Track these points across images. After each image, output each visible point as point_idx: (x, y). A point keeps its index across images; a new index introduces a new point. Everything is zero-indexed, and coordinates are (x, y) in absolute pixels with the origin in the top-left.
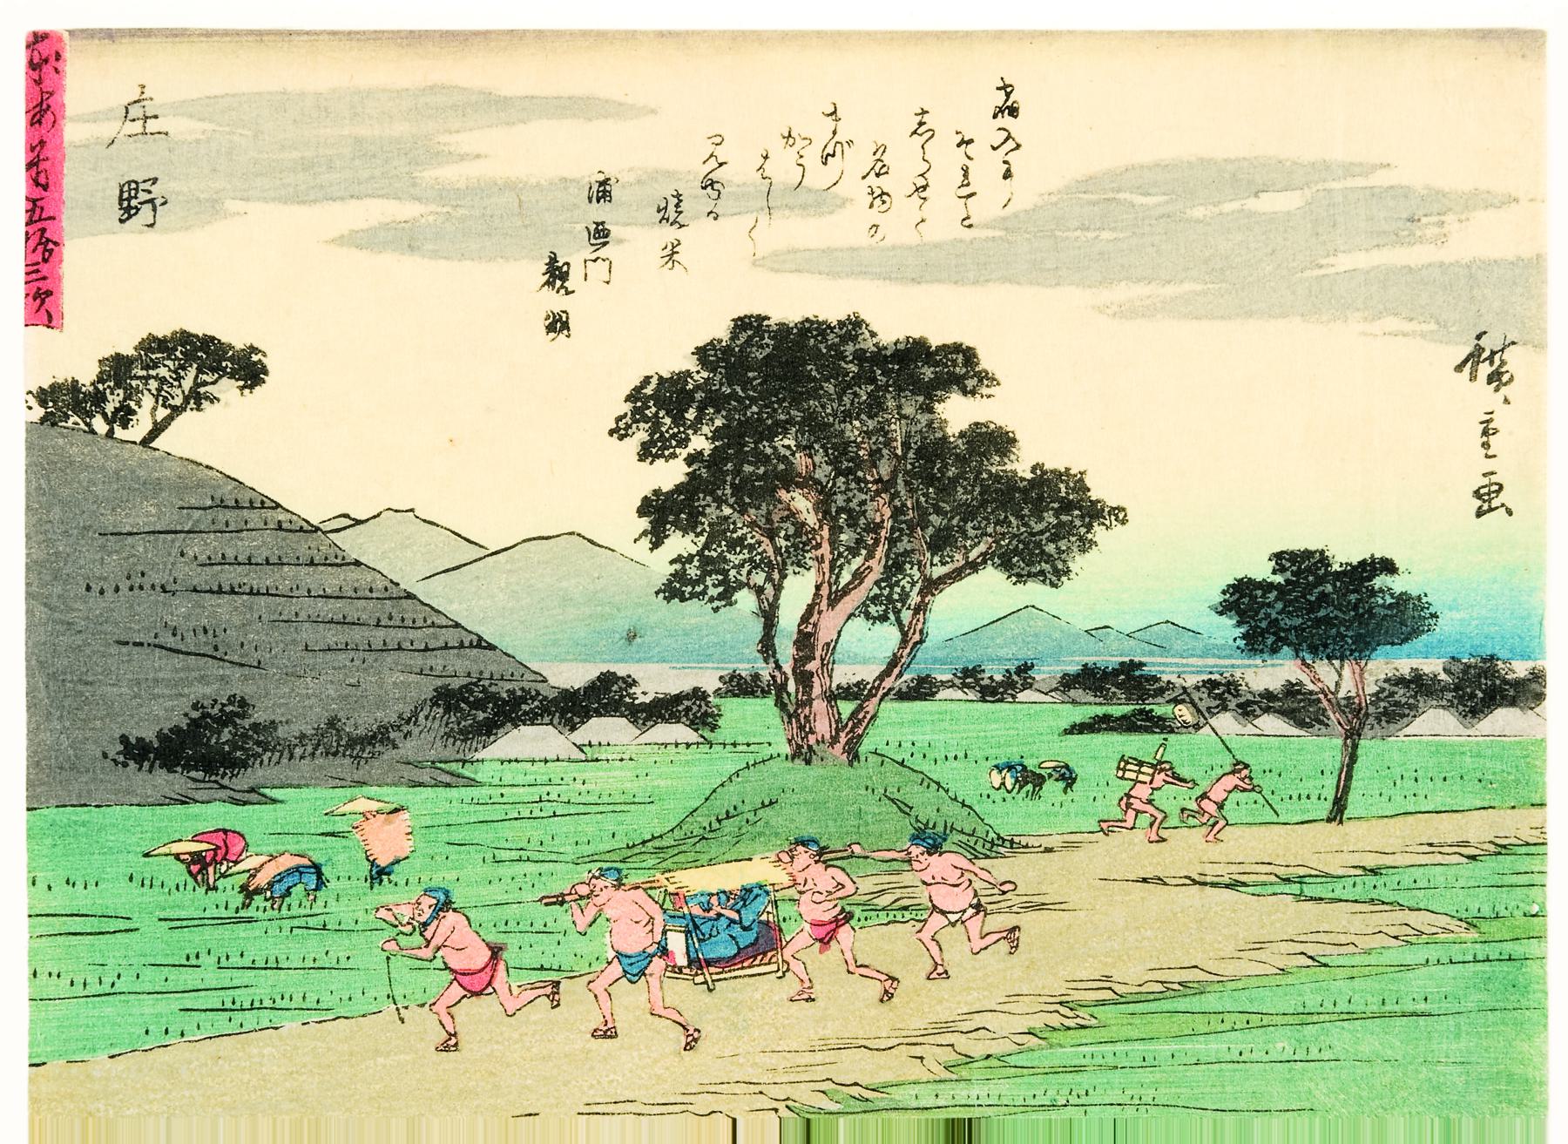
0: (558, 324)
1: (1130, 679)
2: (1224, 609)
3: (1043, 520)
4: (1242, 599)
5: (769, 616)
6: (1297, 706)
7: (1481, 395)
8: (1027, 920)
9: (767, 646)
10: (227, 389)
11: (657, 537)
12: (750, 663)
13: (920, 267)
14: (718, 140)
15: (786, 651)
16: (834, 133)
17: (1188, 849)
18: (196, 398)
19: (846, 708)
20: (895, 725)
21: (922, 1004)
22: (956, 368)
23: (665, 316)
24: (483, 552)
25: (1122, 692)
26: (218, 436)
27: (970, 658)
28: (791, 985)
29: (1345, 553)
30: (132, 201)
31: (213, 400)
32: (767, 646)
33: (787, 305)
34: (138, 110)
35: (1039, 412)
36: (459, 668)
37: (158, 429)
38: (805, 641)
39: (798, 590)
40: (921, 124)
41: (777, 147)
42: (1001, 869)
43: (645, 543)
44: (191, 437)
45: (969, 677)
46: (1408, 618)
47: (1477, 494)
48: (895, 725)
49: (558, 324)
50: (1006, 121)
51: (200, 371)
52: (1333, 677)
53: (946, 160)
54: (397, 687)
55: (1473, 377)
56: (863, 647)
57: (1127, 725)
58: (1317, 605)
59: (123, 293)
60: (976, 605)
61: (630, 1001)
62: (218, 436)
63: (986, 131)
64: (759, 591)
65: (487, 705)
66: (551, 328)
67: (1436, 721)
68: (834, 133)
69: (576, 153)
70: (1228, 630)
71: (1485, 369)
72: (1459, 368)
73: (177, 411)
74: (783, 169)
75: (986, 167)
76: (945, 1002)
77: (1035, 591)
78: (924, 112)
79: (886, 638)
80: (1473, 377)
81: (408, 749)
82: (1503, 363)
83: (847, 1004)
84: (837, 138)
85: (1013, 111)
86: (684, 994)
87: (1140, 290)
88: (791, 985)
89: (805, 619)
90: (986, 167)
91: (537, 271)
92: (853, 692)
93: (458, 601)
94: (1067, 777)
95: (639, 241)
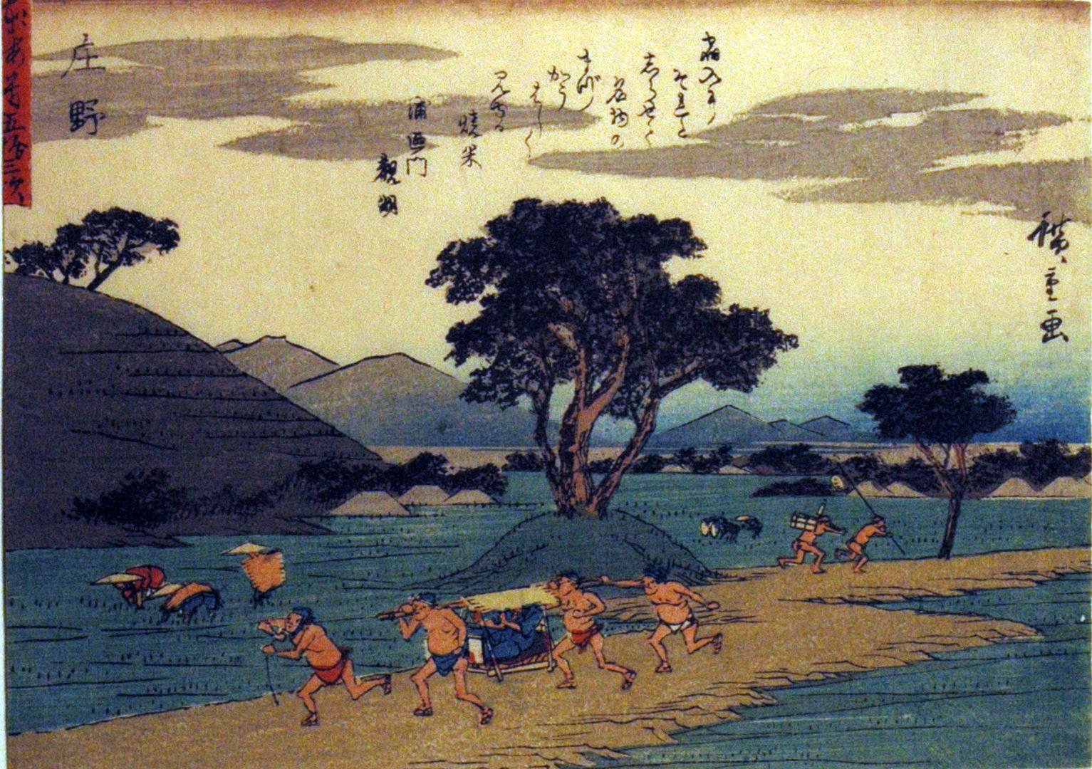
0: (388, 205)
3: (743, 343)
4: (878, 399)
5: (541, 411)
6: (916, 475)
7: (1047, 256)
8: (731, 630)
11: (460, 356)
14: (502, 75)
15: (554, 437)
16: (587, 70)
17: (841, 578)
18: (129, 257)
19: (598, 479)
22: (678, 237)
25: (793, 464)
26: (141, 283)
29: (953, 366)
30: (82, 118)
36: (317, 450)
37: (100, 278)
38: (568, 430)
39: (563, 394)
40: (649, 64)
41: (545, 80)
42: (708, 593)
47: (1043, 326)
48: (634, 491)
49: (388, 205)
50: (710, 63)
51: (130, 237)
52: (945, 456)
54: (272, 461)
55: (1041, 244)
56: (611, 433)
60: (691, 401)
61: (442, 690)
62: (141, 283)
63: (696, 70)
64: (534, 395)
66: (383, 208)
68: (587, 70)
70: (869, 422)
71: (1049, 238)
72: (1031, 237)
73: (113, 266)
75: (696, 94)
76: (672, 688)
78: (651, 56)
79: (628, 427)
80: (1041, 244)
81: (283, 507)
84: (589, 74)
85: (715, 56)
88: (558, 677)
89: (569, 413)
90: (696, 94)
94: (755, 527)
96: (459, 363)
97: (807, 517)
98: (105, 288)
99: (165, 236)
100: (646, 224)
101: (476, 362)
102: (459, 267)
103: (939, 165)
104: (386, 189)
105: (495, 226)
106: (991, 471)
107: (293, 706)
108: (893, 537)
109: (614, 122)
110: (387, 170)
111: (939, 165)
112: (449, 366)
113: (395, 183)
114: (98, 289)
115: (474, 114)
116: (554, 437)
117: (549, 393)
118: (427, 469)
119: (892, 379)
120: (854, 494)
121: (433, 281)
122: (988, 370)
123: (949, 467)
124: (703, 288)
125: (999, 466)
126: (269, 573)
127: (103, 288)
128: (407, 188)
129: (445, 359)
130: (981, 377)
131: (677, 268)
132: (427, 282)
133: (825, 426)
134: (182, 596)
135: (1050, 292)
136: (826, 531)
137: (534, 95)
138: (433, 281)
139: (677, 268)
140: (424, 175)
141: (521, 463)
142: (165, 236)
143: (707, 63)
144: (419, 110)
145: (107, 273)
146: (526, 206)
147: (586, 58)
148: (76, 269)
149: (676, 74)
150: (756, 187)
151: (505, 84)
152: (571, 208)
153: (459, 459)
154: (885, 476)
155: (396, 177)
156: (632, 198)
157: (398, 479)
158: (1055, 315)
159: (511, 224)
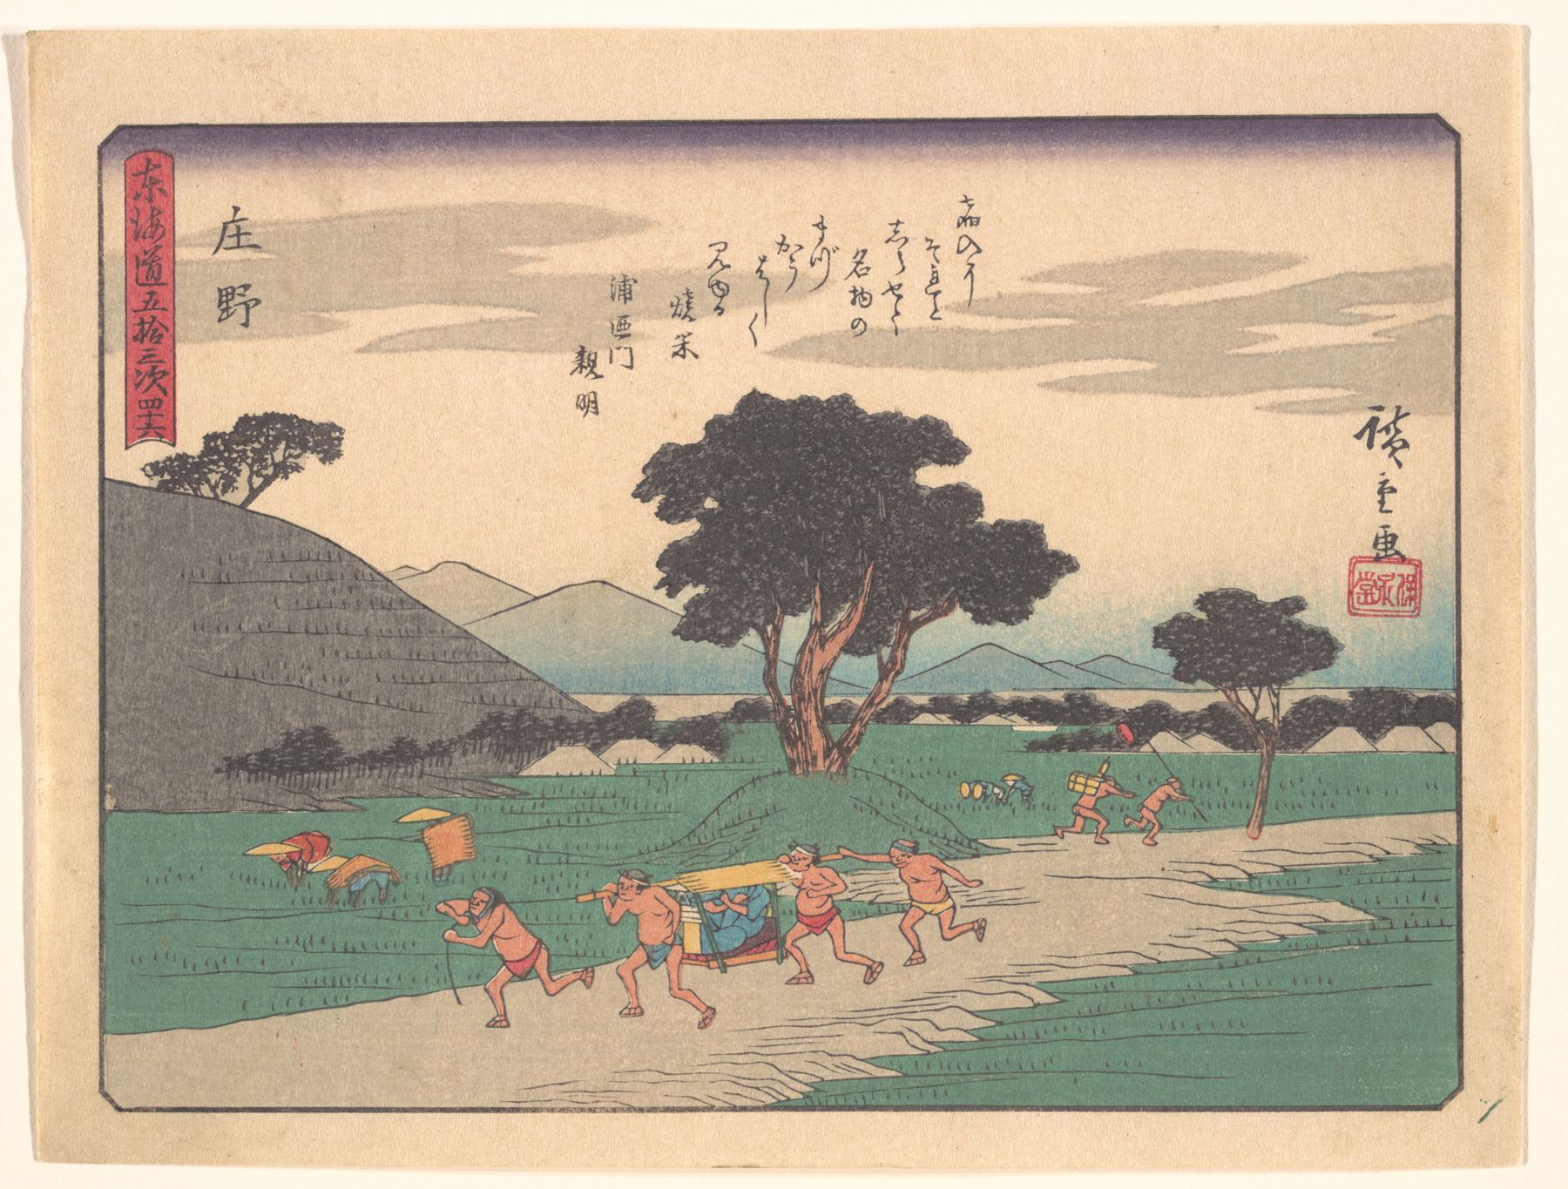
1: (1080, 709)
2: (1156, 645)
3: (1015, 568)
4: (1169, 635)
6: (1217, 722)
8: (993, 916)
9: (770, 680)
10: (311, 461)
11: (671, 586)
12: (756, 691)
13: (902, 348)
14: (722, 247)
15: (784, 674)
16: (821, 240)
18: (283, 470)
20: (877, 740)
21: (894, 986)
23: (684, 391)
24: (526, 598)
25: (1076, 720)
26: (300, 498)
27: (943, 689)
28: (791, 967)
30: (232, 301)
31: (297, 468)
32: (770, 680)
33: (789, 382)
34: (234, 232)
35: (1018, 454)
37: (254, 493)
40: (896, 232)
41: (772, 252)
43: (663, 591)
44: (282, 500)
45: (939, 705)
46: (1322, 649)
48: (877, 740)
49: (588, 404)
50: (971, 231)
51: (288, 447)
52: (1262, 705)
53: (917, 256)
54: (451, 714)
55: (1370, 446)
57: (1077, 745)
58: (1237, 637)
59: (216, 386)
60: (947, 640)
61: (653, 982)
62: (300, 498)
63: (948, 237)
64: (762, 632)
65: (523, 725)
67: (1344, 739)
68: (821, 240)
69: (609, 258)
70: (1164, 661)
72: (1359, 436)
73: (268, 481)
74: (777, 266)
75: (952, 270)
76: (918, 982)
77: (999, 632)
78: (898, 223)
80: (1370, 446)
82: (1398, 431)
83: (838, 985)
84: (824, 244)
85: (975, 222)
86: (694, 975)
87: (1122, 365)
90: (952, 270)
91: (570, 358)
92: (842, 713)
93: (494, 635)
95: (656, 333)
96: (671, 594)
97: (1089, 776)
98: (254, 506)
99: (324, 440)
100: (890, 423)
101: (689, 592)
102: (670, 478)
103: (1266, 338)
104: (583, 383)
105: (715, 426)
106: (1316, 718)
107: (477, 1002)
108: (1195, 806)
109: (853, 302)
110: (585, 362)
111: (1266, 338)
112: (660, 596)
113: (597, 377)
114: (250, 507)
115: (688, 293)
116: (784, 674)
117: (777, 631)
118: (634, 720)
119: (1187, 606)
120: (1146, 748)
121: (642, 494)
122: (1305, 592)
123: (1258, 717)
124: (965, 500)
125: (1316, 718)
126: (451, 842)
127: (254, 506)
128: (612, 383)
129: (657, 588)
130: (1298, 604)
131: (931, 476)
132: (635, 495)
133: (1111, 666)
134: (346, 873)
135: (1382, 502)
136: (1109, 793)
137: (759, 270)
138: (642, 494)
139: (931, 476)
140: (631, 367)
141: (746, 712)
142: (324, 440)
143: (965, 230)
144: (624, 289)
145: (261, 489)
146: (754, 402)
147: (821, 226)
148: (229, 484)
149: (962, 210)
150: (1010, 377)
151: (726, 258)
152: (807, 404)
153: (669, 710)
154: (1184, 725)
155: (598, 370)
156: (881, 391)
157: (600, 732)
158: (1389, 531)
159: (732, 428)
